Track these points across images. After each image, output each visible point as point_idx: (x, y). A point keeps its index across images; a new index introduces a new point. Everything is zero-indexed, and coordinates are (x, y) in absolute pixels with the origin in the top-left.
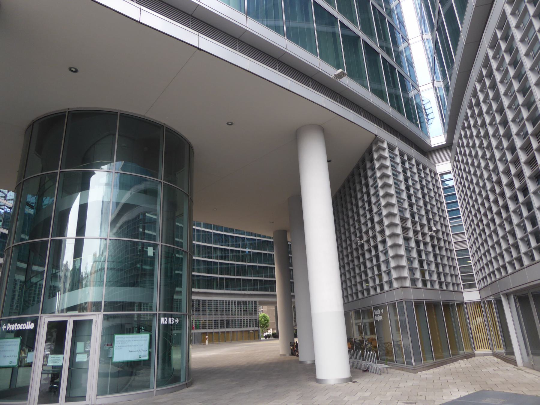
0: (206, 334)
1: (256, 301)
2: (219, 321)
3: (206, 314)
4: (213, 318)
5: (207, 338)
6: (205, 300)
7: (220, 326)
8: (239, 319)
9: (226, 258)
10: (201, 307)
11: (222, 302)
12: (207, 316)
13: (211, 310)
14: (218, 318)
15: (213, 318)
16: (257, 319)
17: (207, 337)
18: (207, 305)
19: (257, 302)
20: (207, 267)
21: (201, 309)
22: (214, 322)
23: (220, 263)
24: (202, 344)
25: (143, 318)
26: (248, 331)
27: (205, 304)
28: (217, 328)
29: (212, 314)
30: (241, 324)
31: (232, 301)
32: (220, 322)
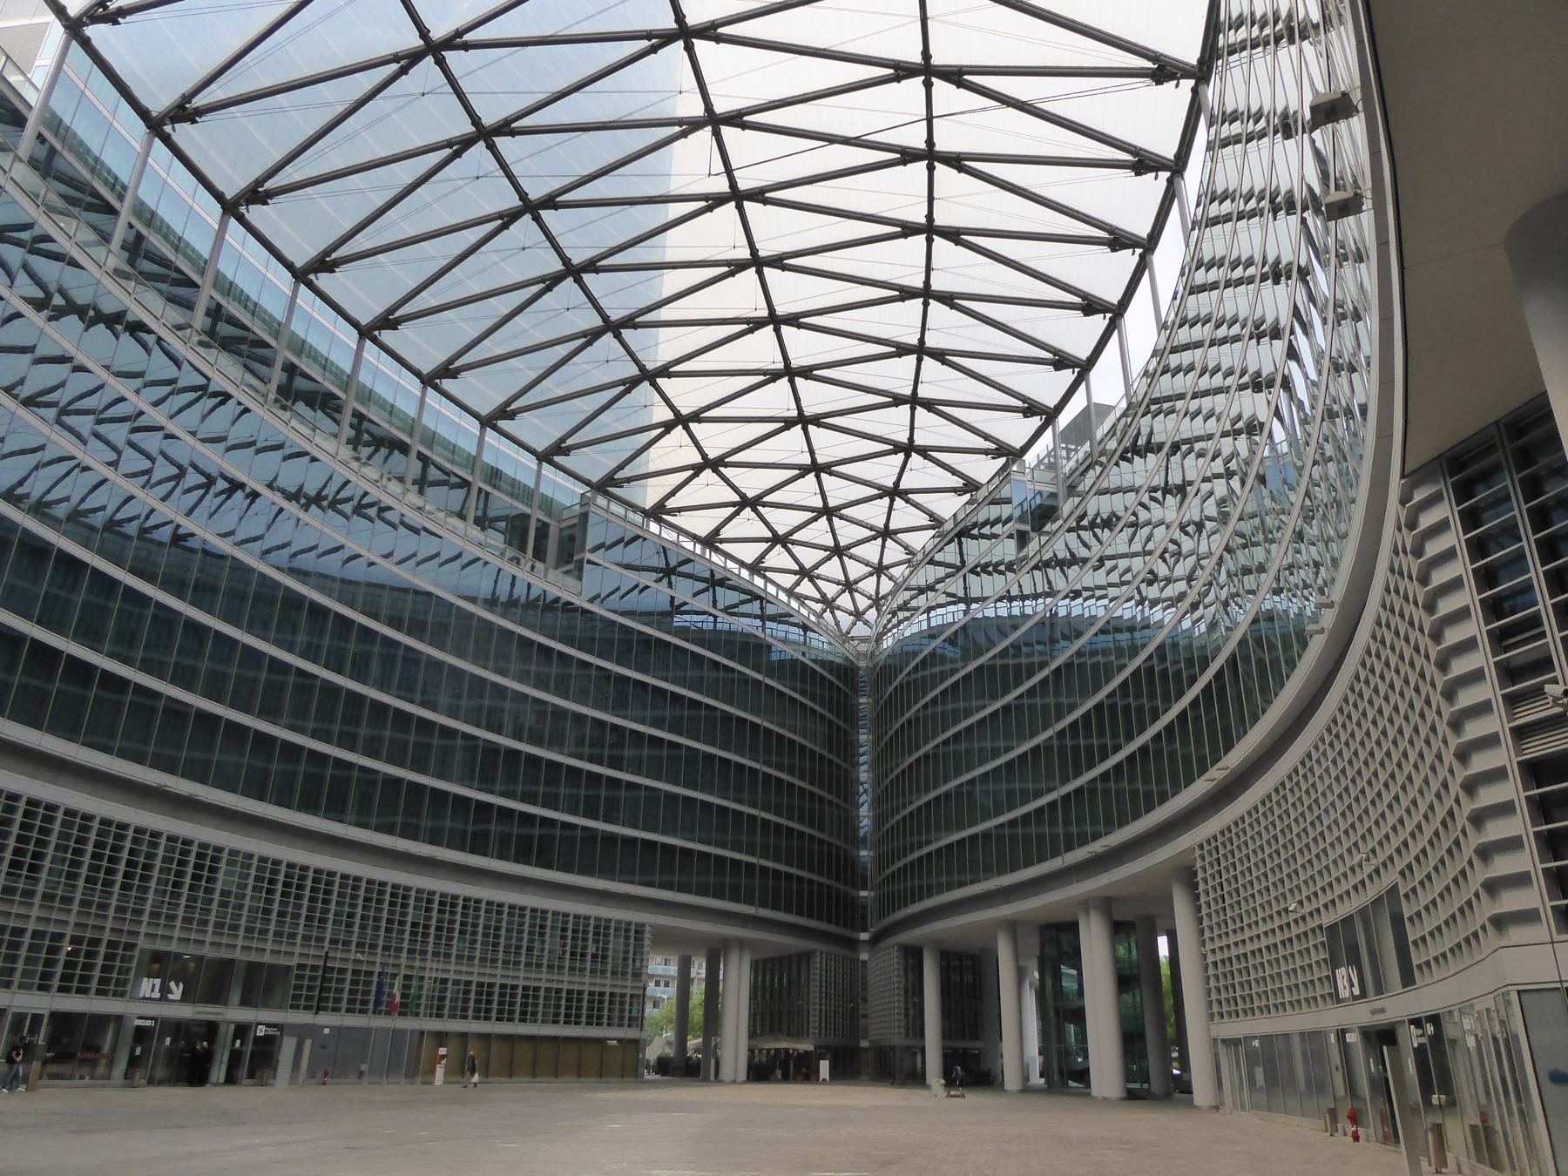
0: (441, 1037)
1: (644, 925)
2: (497, 990)
3: (563, 967)
4: (476, 974)
5: (443, 1057)
6: (123, 826)
7: (567, 1016)
8: (593, 989)
9: (556, 742)
10: (278, 897)
11: (210, 852)
12: (36, 907)
13: (474, 942)
14: (28, 917)
15: (71, 926)
16: (638, 996)
17: (443, 1051)
18: (307, 893)
19: (647, 928)
20: (583, 792)
21: (304, 912)
22: (501, 995)
23: (444, 729)
24: (419, 1079)
25: (180, 939)
26: (601, 1041)
27: (39, 843)
28: (576, 1023)
29: (471, 958)
30: (466, 1001)
31: (619, 922)
32: (523, 996)
